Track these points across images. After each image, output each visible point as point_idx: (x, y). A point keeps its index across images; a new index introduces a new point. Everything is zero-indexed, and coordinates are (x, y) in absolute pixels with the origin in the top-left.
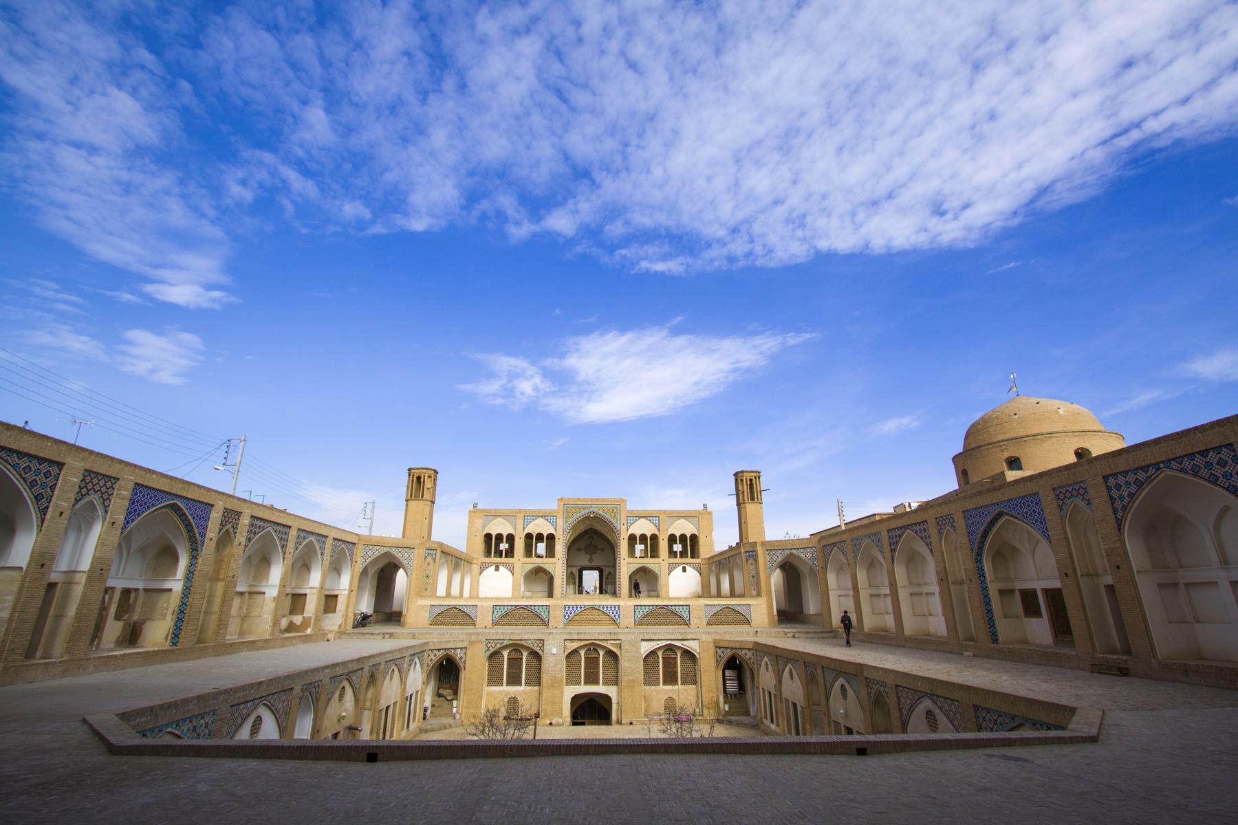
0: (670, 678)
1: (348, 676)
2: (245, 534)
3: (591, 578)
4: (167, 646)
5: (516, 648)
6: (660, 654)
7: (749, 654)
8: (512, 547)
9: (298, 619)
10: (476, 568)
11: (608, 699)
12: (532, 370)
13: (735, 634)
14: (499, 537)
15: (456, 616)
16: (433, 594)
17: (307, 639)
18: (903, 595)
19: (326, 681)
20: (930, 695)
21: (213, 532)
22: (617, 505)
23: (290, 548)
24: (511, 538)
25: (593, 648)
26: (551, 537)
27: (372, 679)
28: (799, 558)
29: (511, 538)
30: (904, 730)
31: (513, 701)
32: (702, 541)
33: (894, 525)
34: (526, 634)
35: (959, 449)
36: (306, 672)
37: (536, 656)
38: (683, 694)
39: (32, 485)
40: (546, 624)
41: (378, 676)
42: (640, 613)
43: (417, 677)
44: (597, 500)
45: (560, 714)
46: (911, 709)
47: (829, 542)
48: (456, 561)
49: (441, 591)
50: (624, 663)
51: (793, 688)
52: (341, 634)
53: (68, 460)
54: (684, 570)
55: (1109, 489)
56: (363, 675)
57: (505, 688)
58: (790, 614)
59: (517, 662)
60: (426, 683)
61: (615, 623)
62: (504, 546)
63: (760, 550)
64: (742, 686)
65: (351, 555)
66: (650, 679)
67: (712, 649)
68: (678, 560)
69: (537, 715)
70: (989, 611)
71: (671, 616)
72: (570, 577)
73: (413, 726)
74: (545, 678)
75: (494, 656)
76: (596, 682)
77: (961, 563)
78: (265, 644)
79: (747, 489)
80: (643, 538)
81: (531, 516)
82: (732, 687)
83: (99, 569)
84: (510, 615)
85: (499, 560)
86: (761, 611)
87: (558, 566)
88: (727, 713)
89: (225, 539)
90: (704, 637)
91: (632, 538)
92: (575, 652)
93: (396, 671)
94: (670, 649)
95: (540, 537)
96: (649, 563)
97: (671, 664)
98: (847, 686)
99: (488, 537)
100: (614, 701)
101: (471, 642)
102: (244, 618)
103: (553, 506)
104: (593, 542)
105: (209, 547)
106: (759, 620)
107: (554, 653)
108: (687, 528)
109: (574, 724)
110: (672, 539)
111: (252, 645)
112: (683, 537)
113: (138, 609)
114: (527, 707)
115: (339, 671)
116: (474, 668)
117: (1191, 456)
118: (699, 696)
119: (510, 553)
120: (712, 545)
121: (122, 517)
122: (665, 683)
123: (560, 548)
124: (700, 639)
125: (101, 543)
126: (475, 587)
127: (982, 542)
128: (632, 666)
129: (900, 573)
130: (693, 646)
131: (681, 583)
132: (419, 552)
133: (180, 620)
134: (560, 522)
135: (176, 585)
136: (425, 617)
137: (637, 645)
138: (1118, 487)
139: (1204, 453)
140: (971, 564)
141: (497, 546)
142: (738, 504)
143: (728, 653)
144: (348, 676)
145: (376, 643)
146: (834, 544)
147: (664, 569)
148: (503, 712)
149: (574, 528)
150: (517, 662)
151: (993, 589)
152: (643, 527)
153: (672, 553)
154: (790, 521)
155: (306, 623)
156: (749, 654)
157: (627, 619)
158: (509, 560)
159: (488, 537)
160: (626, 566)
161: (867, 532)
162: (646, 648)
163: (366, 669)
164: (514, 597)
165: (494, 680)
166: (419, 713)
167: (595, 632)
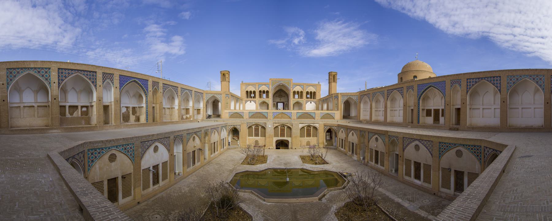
0: (309, 135)
1: (195, 133)
3: (280, 105)
4: (145, 122)
5: (257, 125)
6: (305, 128)
7: (336, 128)
8: (255, 95)
9: (188, 116)
10: (244, 102)
11: (288, 141)
12: (302, 32)
13: (330, 122)
14: (251, 92)
15: (237, 115)
16: (230, 109)
17: (191, 121)
18: (373, 110)
19: (185, 135)
20: (419, 140)
21: (150, 88)
22: (290, 80)
23: (179, 94)
24: (254, 92)
25: (283, 126)
26: (268, 92)
27: (206, 134)
28: (352, 99)
29: (254, 92)
31: (257, 142)
32: (317, 94)
33: (390, 88)
34: (261, 121)
36: (175, 132)
37: (264, 128)
38: (313, 140)
39: (90, 79)
40: (267, 118)
41: (209, 133)
42: (299, 115)
43: (225, 134)
45: (272, 146)
47: (363, 95)
48: (237, 99)
49: (232, 107)
50: (293, 131)
51: (353, 138)
52: (202, 120)
53: (97, 70)
55: (467, 82)
56: (205, 133)
57: (254, 137)
58: (346, 116)
59: (258, 130)
60: (229, 135)
61: (290, 118)
62: (253, 95)
63: (340, 96)
64: (331, 138)
65: (202, 97)
66: (302, 135)
67: (323, 127)
68: (309, 100)
69: (265, 146)
70: (419, 115)
71: (308, 116)
72: (274, 104)
73: (225, 147)
74: (267, 135)
75: (250, 127)
76: (284, 136)
77: (412, 102)
78: (177, 122)
80: (298, 92)
81: (261, 85)
82: (328, 138)
83: (118, 101)
84: (254, 115)
86: (338, 115)
87: (270, 101)
88: (326, 145)
89: (155, 92)
90: (320, 123)
91: (294, 92)
92: (277, 127)
94: (309, 126)
95: (264, 92)
96: (300, 100)
97: (309, 131)
98: (379, 138)
99: (247, 92)
100: (290, 142)
101: (242, 123)
102: (171, 115)
104: (281, 94)
105: (150, 94)
106: (337, 118)
107: (270, 127)
108: (312, 89)
109: (277, 148)
110: (307, 93)
111: (172, 123)
112: (311, 92)
113: (138, 112)
114: (261, 143)
115: (191, 131)
116: (244, 131)
117: (491, 77)
118: (318, 140)
119: (254, 97)
120: (320, 95)
122: (307, 136)
123: (271, 95)
124: (320, 124)
125: (115, 93)
126: (244, 107)
127: (422, 95)
128: (296, 131)
129: (389, 103)
130: (317, 125)
131: (310, 106)
132: (223, 96)
133: (147, 115)
134: (270, 86)
135: (144, 105)
136: (227, 116)
137: (298, 125)
138: (470, 82)
139: (494, 77)
140: (417, 101)
141: (250, 95)
142: (329, 83)
143: (328, 128)
144: (195, 133)
145: (213, 122)
146: (365, 95)
147: (305, 103)
148: (253, 145)
149: (275, 89)
150: (258, 130)
151: (421, 108)
153: (307, 98)
154: (347, 86)
155: (190, 116)
156: (336, 128)
157: (294, 117)
159: (247, 92)
160: (292, 101)
161: (379, 90)
162: (301, 126)
163: (203, 131)
164: (256, 110)
165: (250, 135)
166: (227, 144)
167: (284, 121)
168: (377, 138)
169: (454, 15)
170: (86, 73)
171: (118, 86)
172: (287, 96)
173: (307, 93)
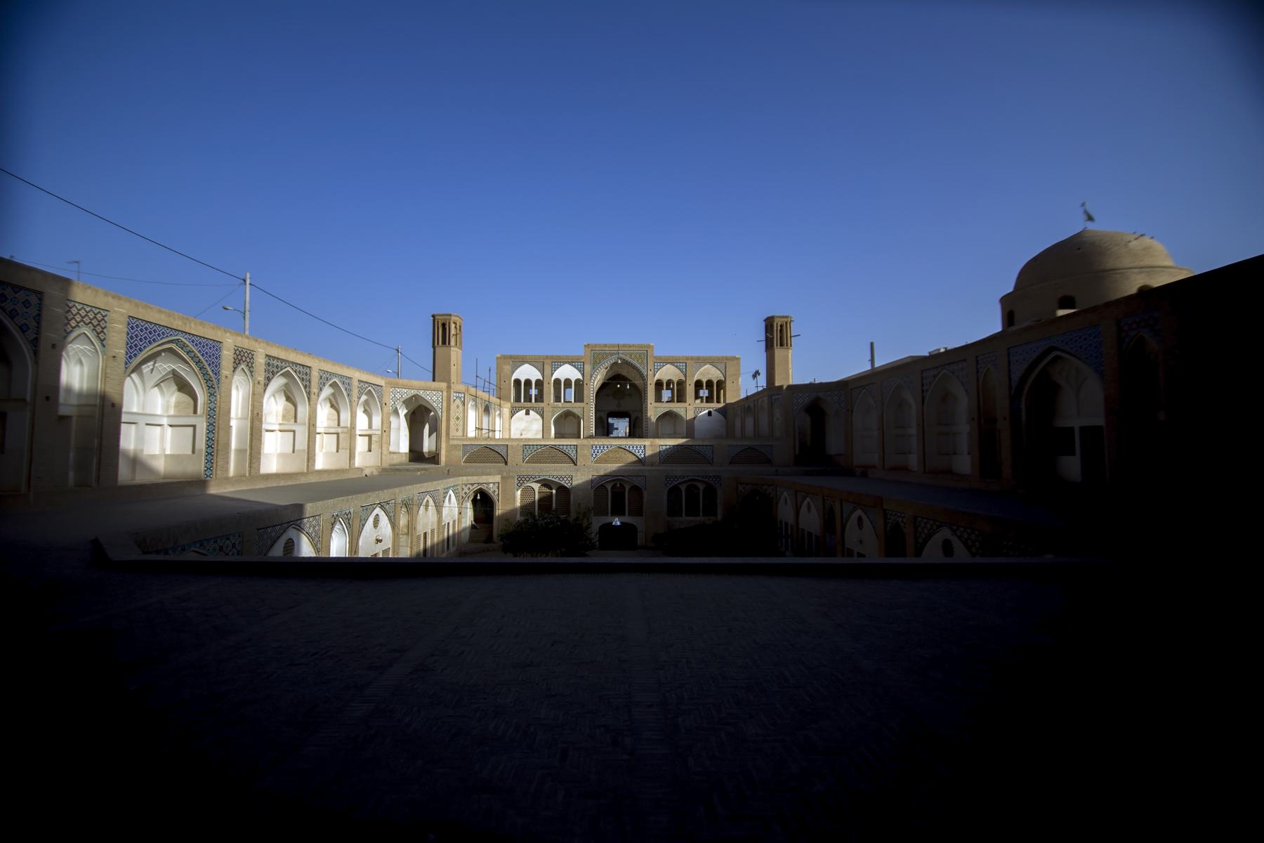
2: (263, 374)
3: (622, 426)
22: (645, 351)
30: (918, 553)
35: (1010, 288)
39: (302, 380)
44: (624, 346)
46: (929, 536)
54: (527, 413)
79: (775, 334)
84: (537, 453)
85: (528, 404)
87: (588, 412)
91: (659, 384)
93: (431, 502)
98: (864, 518)
103: (579, 351)
108: (709, 373)
110: (698, 385)
112: (710, 383)
120: (738, 390)
121: (123, 352)
152: (668, 373)
153: (697, 396)
158: (541, 405)
160: (653, 410)
168: (860, 519)
169: (743, 428)
170: (298, 368)
171: (121, 352)
172: (638, 393)
173: (698, 385)
